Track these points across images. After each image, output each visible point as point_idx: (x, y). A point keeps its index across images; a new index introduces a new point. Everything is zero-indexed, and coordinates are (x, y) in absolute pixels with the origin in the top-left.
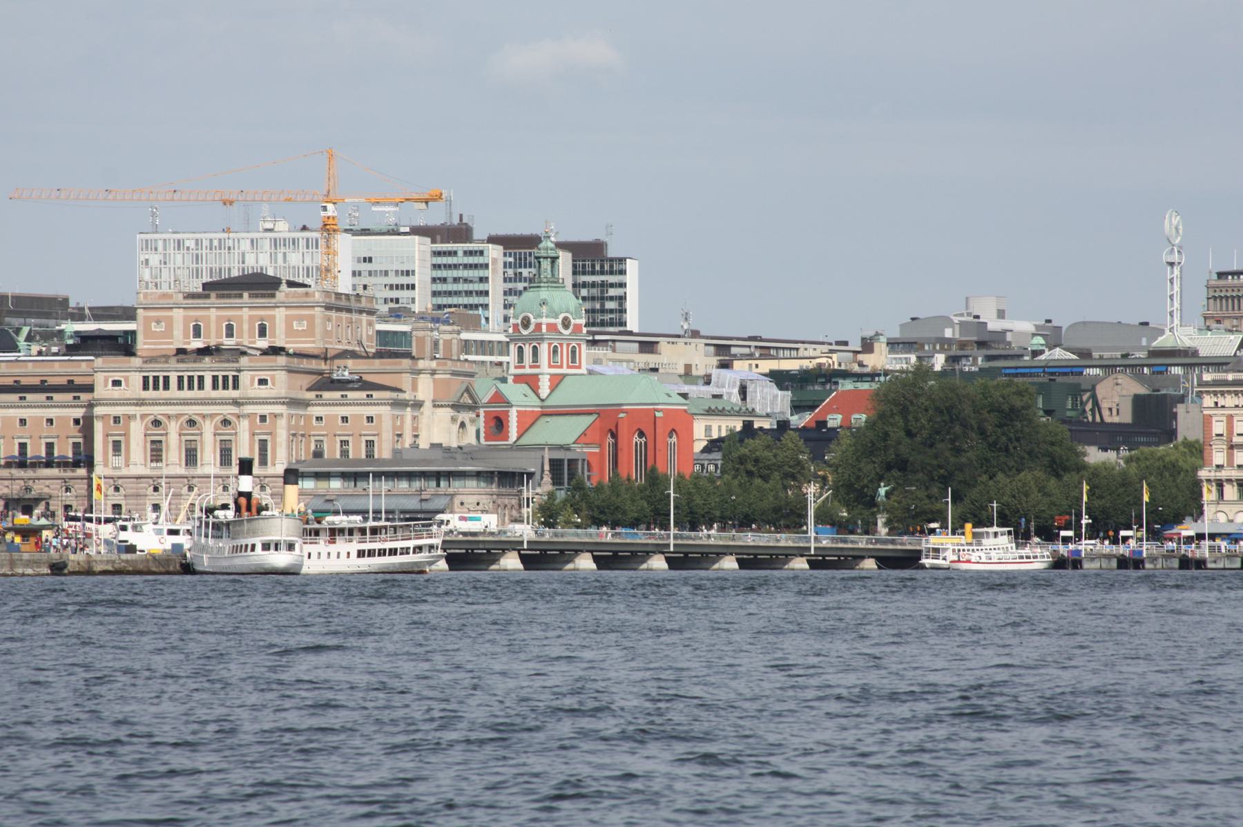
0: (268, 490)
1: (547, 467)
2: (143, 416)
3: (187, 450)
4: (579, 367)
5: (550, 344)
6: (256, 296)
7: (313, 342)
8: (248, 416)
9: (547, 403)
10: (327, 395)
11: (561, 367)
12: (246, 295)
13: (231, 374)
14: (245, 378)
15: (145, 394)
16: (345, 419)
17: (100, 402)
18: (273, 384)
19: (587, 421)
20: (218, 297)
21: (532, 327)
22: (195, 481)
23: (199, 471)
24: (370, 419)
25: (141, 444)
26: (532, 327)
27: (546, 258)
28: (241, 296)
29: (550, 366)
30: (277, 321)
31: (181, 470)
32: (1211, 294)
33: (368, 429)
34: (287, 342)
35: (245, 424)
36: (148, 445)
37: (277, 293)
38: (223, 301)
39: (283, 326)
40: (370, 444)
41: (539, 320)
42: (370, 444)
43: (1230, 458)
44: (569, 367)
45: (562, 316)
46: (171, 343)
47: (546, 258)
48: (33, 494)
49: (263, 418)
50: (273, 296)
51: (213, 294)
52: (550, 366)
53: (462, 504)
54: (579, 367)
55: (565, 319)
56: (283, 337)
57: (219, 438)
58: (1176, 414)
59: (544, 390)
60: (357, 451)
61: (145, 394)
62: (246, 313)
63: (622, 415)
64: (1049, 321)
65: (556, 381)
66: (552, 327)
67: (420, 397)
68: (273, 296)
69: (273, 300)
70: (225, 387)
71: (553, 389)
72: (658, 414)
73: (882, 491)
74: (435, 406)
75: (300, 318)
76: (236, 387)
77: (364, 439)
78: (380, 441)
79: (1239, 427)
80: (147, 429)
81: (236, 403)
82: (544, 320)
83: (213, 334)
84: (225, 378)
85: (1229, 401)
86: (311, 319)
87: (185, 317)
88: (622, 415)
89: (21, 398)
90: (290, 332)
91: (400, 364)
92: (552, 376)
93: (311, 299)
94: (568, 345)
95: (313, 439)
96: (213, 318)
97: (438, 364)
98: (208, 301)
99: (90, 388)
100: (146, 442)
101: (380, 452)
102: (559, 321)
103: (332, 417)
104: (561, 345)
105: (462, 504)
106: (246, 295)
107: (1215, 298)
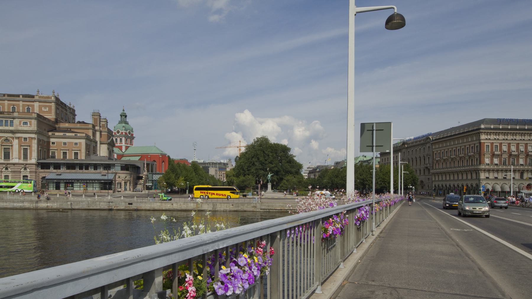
0: (28, 170)
1: (145, 166)
3: (5, 153)
8: (18, 138)
16: (65, 144)
19: (139, 157)
22: (27, 166)
23: (11, 161)
24: (76, 144)
30: (35, 107)
36: (3, 150)
43: (492, 161)
49: (25, 139)
53: (119, 177)
57: (3, 147)
58: (193, 162)
59: (124, 150)
60: (70, 157)
65: (127, 148)
73: (269, 176)
77: (73, 152)
78: (81, 153)
79: (529, 148)
81: (12, 132)
85: (527, 138)
86: (50, 107)
87: (8, 104)
101: (81, 156)
105: (119, 177)
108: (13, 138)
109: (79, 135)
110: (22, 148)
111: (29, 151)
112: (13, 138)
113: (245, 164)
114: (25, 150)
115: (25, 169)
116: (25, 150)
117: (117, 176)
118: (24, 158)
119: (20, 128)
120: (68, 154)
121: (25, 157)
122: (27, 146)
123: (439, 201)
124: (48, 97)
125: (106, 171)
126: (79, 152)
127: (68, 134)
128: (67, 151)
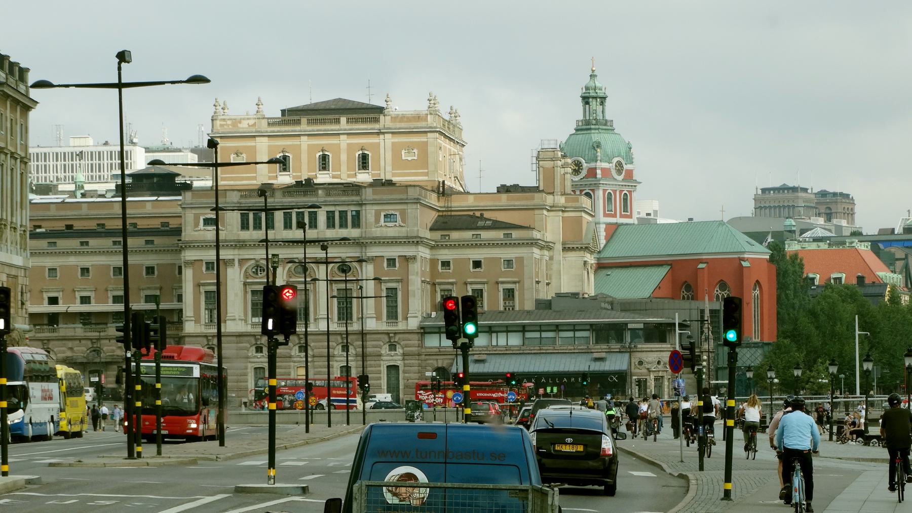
0: (399, 350)
2: (242, 261)
4: (630, 217)
5: (604, 191)
6: (356, 121)
7: (427, 174)
9: (605, 254)
10: (455, 235)
11: (615, 216)
12: (343, 120)
13: (351, 210)
14: (368, 214)
15: (245, 235)
16: (477, 264)
17: (189, 245)
18: (403, 221)
20: (309, 122)
21: (584, 173)
24: (509, 262)
25: (240, 294)
26: (584, 173)
27: (595, 98)
28: (338, 121)
29: (605, 215)
31: (383, 326)
32: (758, 205)
33: (507, 279)
34: (394, 175)
35: (369, 270)
36: (249, 296)
37: (382, 117)
38: (316, 127)
39: (389, 156)
40: (510, 294)
41: (592, 165)
42: (510, 294)
44: (621, 216)
45: (615, 160)
46: (255, 178)
47: (595, 98)
48: (104, 357)
49: (391, 262)
50: (377, 120)
51: (304, 120)
52: (605, 215)
53: (641, 363)
54: (630, 217)
55: (619, 164)
56: (389, 168)
61: (245, 235)
62: (344, 141)
63: (701, 266)
64: (691, 219)
66: (606, 172)
67: (549, 237)
68: (377, 120)
69: (377, 126)
70: (343, 225)
71: (609, 238)
72: (745, 264)
74: (565, 249)
75: (409, 147)
76: (356, 223)
78: (522, 289)
80: (246, 276)
81: (358, 243)
82: (600, 165)
83: (305, 166)
84: (343, 214)
88: (701, 266)
89: (82, 243)
90: (397, 162)
91: (533, 198)
92: (608, 225)
93: (423, 124)
94: (621, 191)
95: (501, 287)
96: (304, 147)
97: (566, 201)
98: (298, 128)
99: (178, 232)
100: (246, 292)
102: (612, 166)
103: (461, 262)
104: (615, 192)
105: (641, 363)
106: (343, 120)
107: (761, 208)
108: (360, 261)
109: (515, 234)
110: (203, 289)
111: (400, 294)
112: (360, 261)
113: (564, 156)
114: (392, 294)
115: (393, 347)
116: (392, 294)
117: (635, 361)
118: (388, 317)
119: (377, 232)
120: (485, 295)
121: (392, 314)
122: (397, 281)
123: (457, 203)
124: (418, 118)
125: (604, 346)
126: (516, 287)
127: (486, 235)
128: (485, 288)
